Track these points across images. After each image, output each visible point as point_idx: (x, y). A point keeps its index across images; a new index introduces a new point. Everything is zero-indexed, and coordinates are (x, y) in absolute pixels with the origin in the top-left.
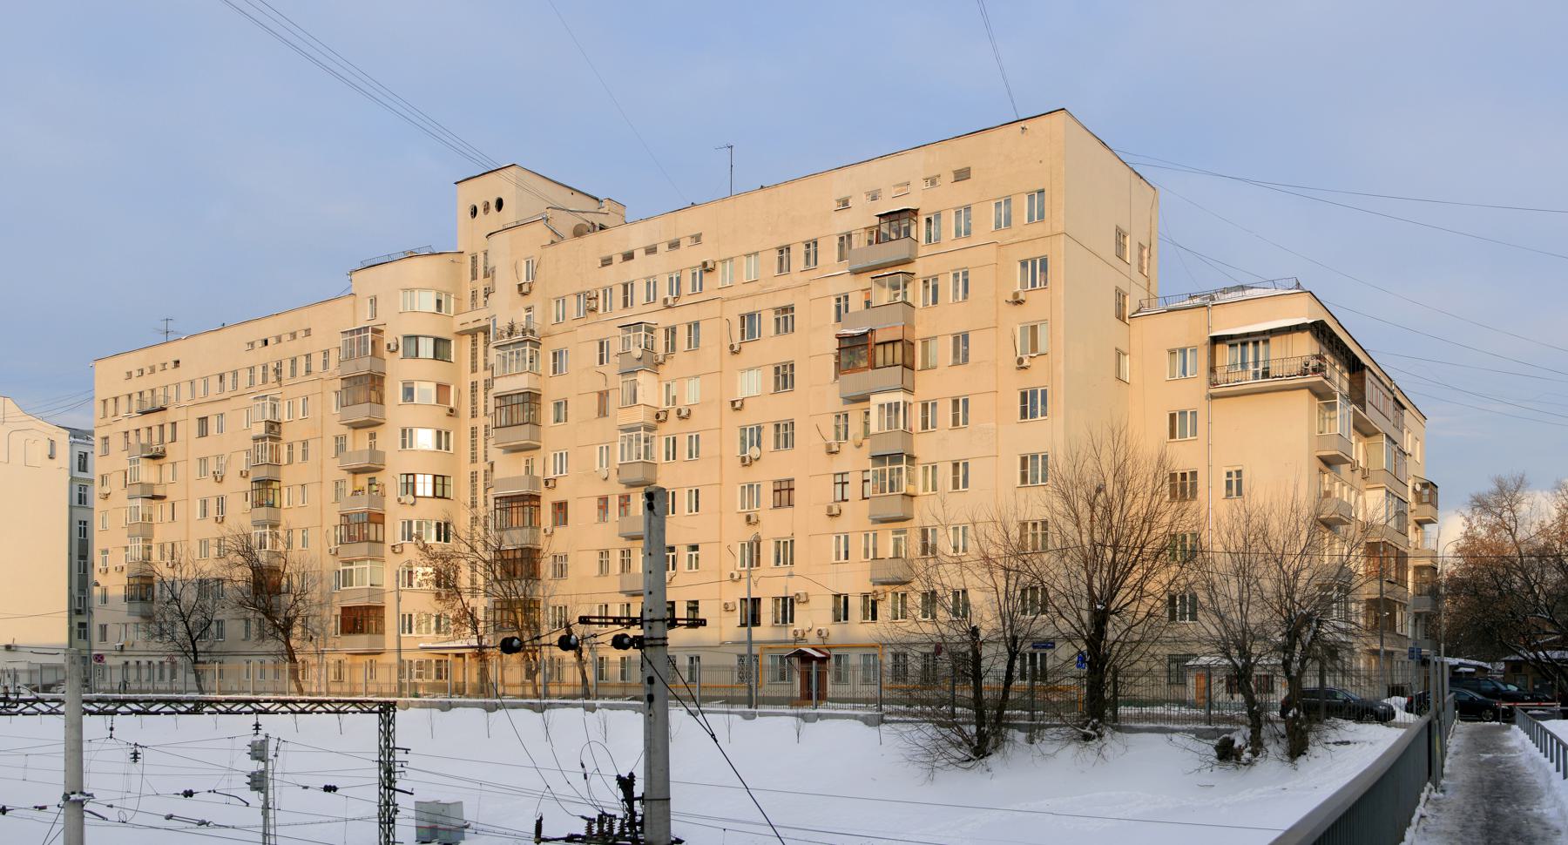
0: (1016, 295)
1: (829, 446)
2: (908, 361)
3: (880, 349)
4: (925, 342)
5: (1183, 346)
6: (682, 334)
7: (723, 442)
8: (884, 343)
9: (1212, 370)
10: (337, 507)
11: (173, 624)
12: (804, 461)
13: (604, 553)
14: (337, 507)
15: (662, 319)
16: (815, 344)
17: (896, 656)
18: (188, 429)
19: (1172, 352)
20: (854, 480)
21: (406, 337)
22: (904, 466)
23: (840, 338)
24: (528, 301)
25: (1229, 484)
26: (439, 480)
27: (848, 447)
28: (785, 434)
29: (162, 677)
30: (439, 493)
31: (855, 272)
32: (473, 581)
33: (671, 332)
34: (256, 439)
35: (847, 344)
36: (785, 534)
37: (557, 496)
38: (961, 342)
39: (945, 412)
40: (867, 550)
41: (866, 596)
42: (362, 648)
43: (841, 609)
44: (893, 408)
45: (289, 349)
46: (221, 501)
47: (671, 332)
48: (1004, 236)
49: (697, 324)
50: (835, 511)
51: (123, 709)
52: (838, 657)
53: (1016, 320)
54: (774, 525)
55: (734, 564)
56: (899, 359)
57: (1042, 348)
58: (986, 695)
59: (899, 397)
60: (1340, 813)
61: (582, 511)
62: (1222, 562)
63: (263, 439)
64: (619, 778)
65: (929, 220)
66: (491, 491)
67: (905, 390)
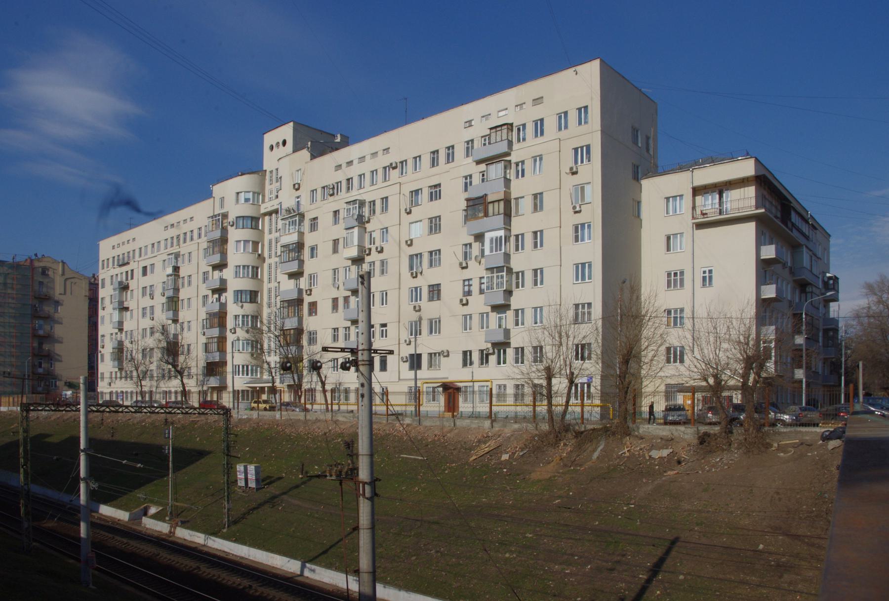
0: (571, 169)
1: (461, 264)
3: (491, 207)
4: (517, 199)
6: (378, 204)
8: (493, 202)
9: (694, 208)
10: (205, 309)
11: (131, 372)
12: (448, 276)
13: (336, 330)
14: (205, 309)
16: (453, 203)
17: (517, 386)
18: (138, 273)
22: (504, 274)
23: (468, 200)
24: (298, 193)
25: (704, 278)
27: (472, 263)
28: (435, 255)
31: (479, 162)
32: (269, 346)
34: (168, 276)
35: (471, 203)
36: (434, 315)
38: (538, 198)
39: (529, 240)
41: (482, 351)
42: (249, 476)
43: (467, 357)
44: (498, 241)
45: (186, 228)
46: (152, 307)
48: (564, 134)
49: (387, 198)
51: (653, 302)
54: (430, 309)
55: (405, 335)
56: (502, 211)
57: (587, 200)
58: (545, 402)
60: (261, 567)
61: (324, 307)
62: (703, 326)
63: (171, 275)
64: (486, 195)
65: (519, 130)
66: (278, 298)
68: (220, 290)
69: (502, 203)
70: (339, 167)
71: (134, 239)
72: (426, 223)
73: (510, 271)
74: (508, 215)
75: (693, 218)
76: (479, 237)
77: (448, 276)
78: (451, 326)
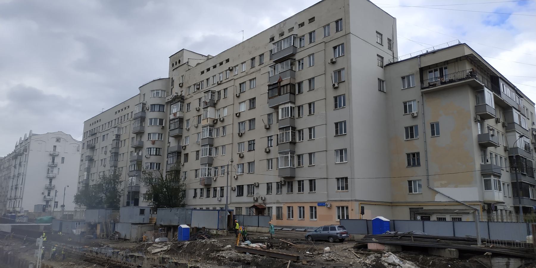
0: (332, 60)
2: (292, 91)
3: (282, 89)
5: (408, 74)
6: (222, 93)
7: (232, 130)
15: (217, 89)
18: (100, 139)
19: (403, 78)
20: (274, 138)
21: (151, 105)
26: (158, 150)
29: (215, 196)
30: (158, 154)
33: (219, 92)
35: (271, 88)
37: (186, 152)
39: (306, 108)
40: (303, 134)
47: (219, 92)
49: (254, 99)
50: (268, 150)
52: (269, 208)
53: (331, 69)
56: (289, 91)
59: (289, 105)
63: (114, 140)
67: (291, 102)
68: (139, 148)
69: (289, 86)
70: (203, 73)
71: (129, 107)
72: (248, 102)
73: (294, 128)
74: (293, 93)
75: (422, 88)
76: (276, 108)
77: (258, 134)
78: (260, 166)
